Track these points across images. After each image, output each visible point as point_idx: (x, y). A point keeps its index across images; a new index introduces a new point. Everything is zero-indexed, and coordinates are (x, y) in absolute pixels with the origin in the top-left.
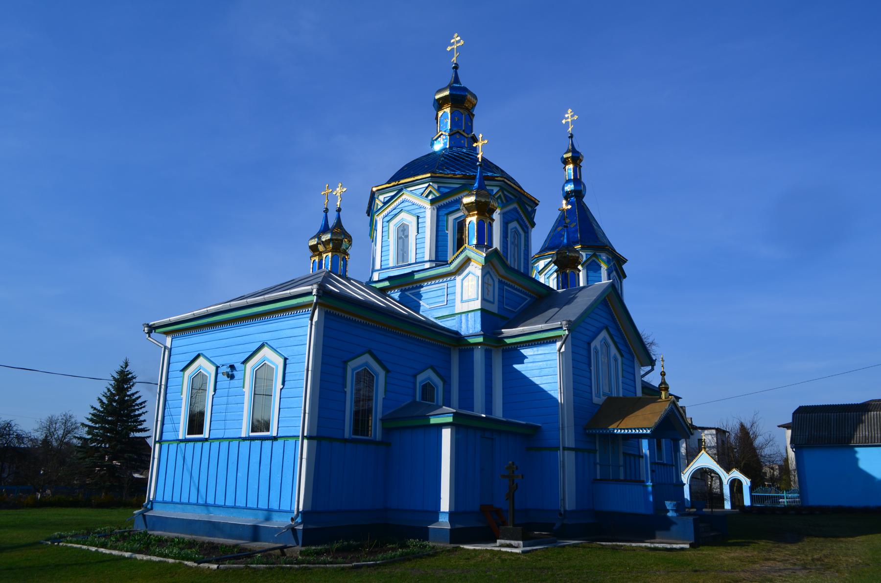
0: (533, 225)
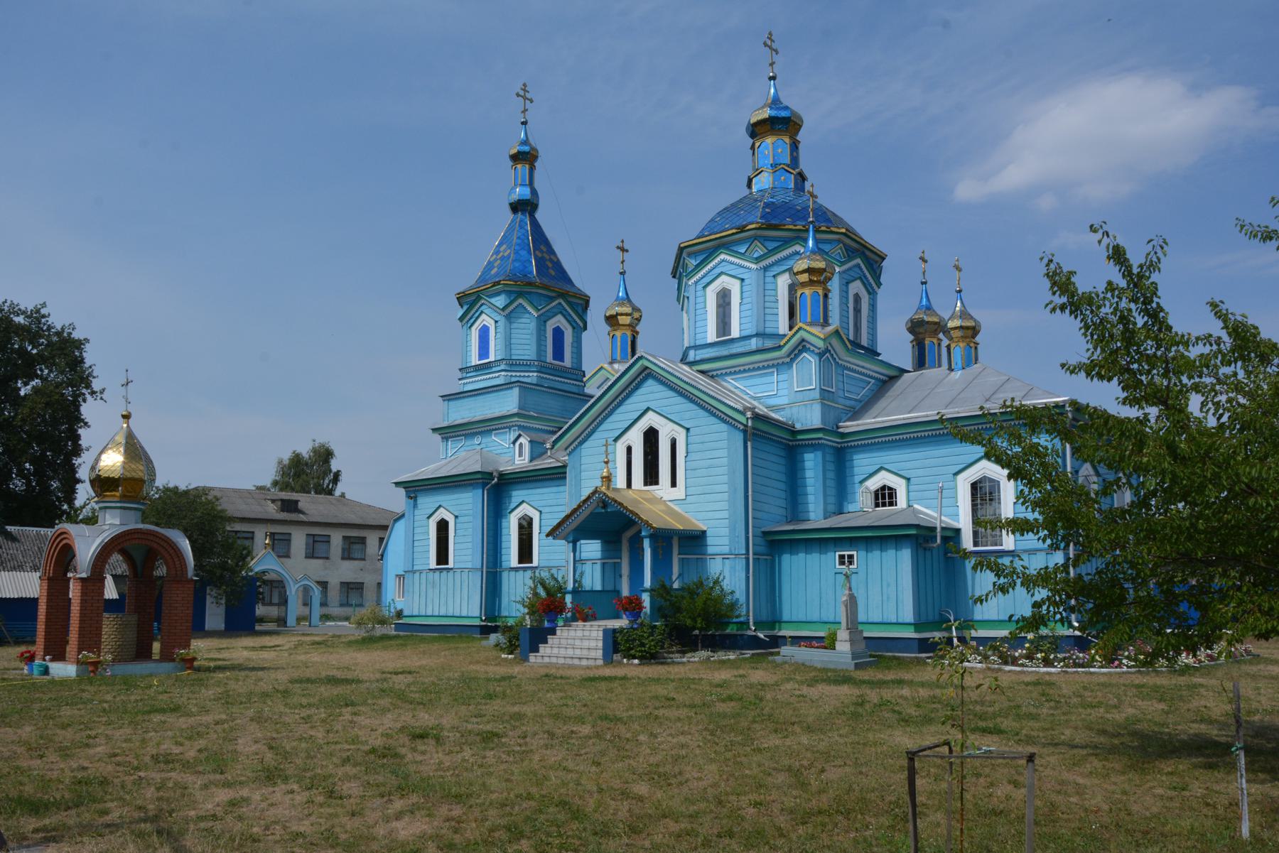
0: (879, 285)
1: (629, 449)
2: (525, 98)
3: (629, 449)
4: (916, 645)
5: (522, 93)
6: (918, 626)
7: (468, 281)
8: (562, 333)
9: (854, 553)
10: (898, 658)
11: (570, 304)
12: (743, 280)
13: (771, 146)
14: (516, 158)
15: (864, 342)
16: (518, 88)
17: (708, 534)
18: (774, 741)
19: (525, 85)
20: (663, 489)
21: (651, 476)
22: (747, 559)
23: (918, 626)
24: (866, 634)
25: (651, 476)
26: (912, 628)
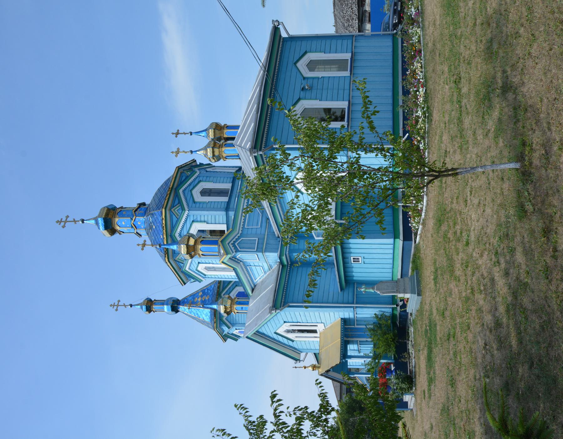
1: (296, 337)
2: (118, 305)
3: (296, 337)
4: (406, 242)
5: (115, 307)
6: (396, 237)
7: (218, 339)
8: (239, 293)
9: (352, 258)
10: (414, 255)
11: (224, 289)
12: (199, 263)
13: (120, 222)
14: (149, 310)
15: (226, 199)
16: (113, 310)
17: (343, 317)
18: (489, 199)
19: (111, 305)
20: (320, 328)
21: (315, 331)
22: (356, 307)
23: (396, 237)
24: (399, 277)
25: (315, 331)
26: (397, 240)
